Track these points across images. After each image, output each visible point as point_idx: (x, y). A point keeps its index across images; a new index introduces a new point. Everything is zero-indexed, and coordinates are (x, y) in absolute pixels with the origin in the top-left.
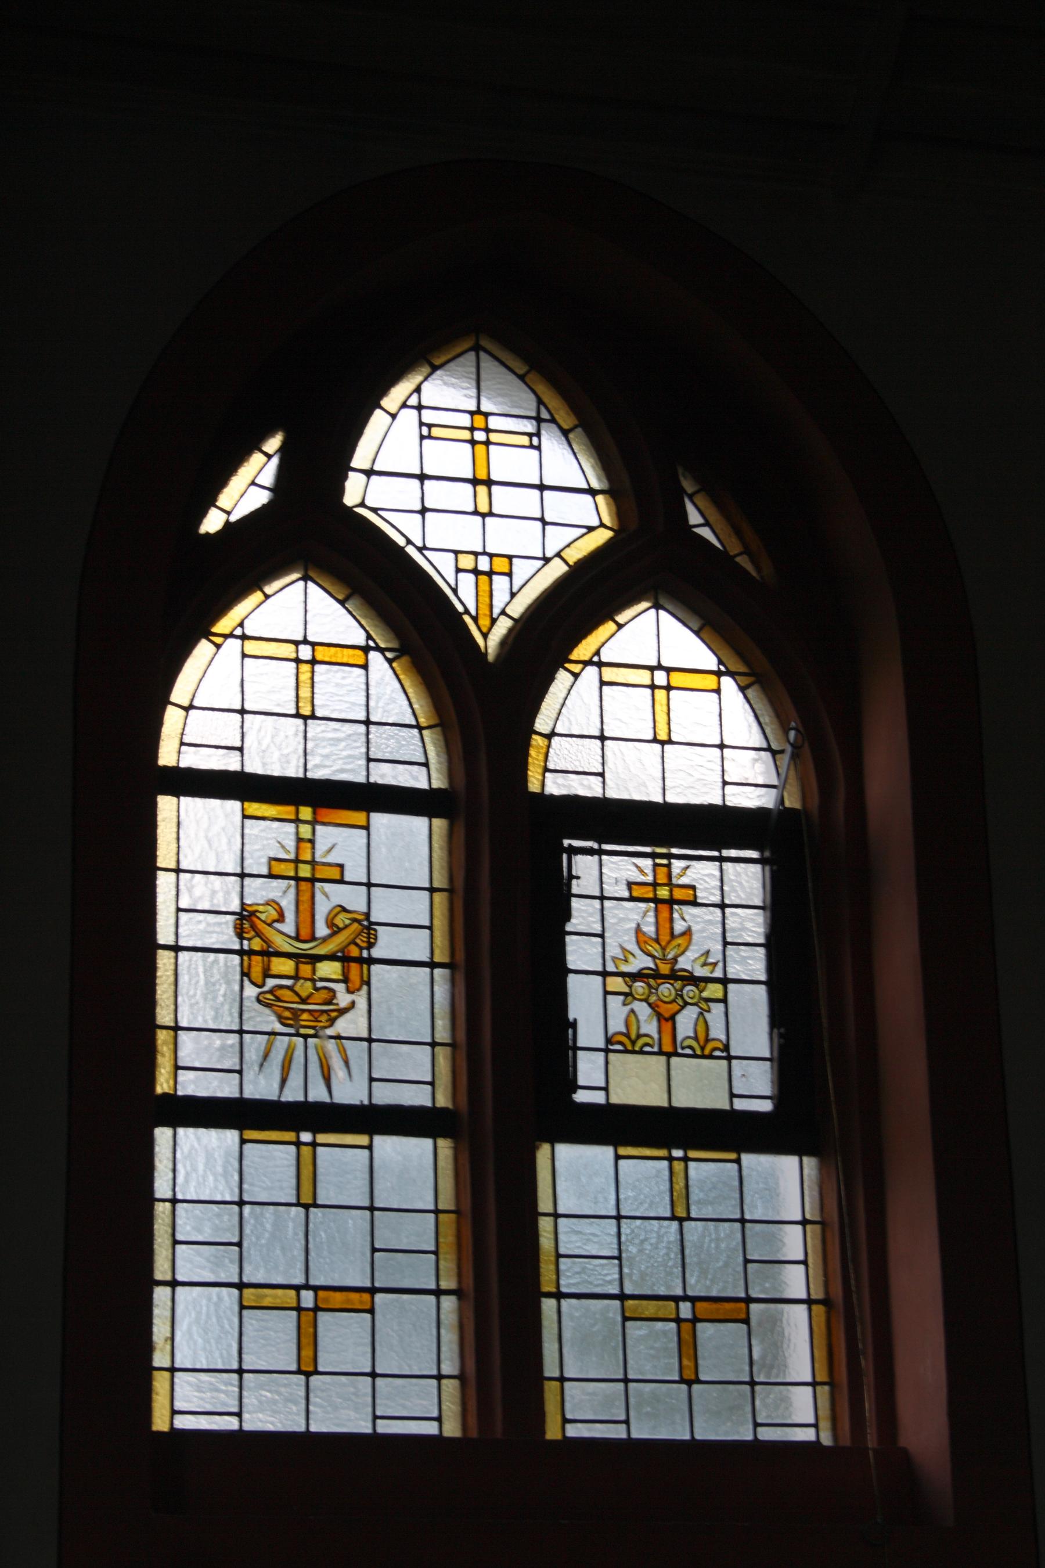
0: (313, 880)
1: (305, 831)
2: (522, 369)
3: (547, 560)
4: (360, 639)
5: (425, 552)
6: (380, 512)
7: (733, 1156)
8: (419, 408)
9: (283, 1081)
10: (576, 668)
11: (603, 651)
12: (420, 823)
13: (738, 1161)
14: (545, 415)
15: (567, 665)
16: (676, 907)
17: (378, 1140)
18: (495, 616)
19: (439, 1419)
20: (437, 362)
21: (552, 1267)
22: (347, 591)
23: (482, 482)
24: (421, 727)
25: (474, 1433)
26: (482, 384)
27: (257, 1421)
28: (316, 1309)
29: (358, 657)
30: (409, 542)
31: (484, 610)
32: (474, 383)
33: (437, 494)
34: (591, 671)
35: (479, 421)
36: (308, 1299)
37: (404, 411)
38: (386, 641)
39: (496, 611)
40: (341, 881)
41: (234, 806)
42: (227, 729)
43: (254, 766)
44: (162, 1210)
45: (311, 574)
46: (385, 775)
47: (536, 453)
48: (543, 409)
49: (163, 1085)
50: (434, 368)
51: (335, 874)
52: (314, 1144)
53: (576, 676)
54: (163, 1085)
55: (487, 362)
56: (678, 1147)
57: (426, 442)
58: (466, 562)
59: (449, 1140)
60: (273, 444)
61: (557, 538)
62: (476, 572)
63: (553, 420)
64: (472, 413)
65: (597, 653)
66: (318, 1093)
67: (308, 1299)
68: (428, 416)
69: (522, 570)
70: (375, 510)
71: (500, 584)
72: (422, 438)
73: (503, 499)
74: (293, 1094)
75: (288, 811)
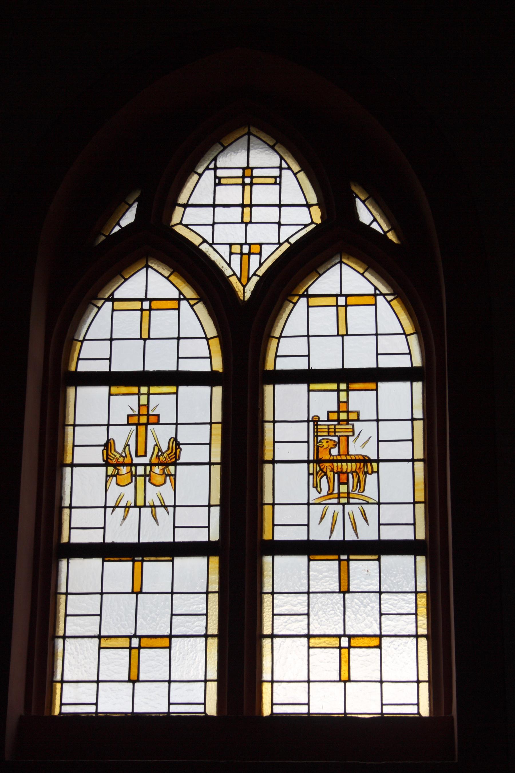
1: (343, 396)
3: (280, 244)
4: (175, 294)
6: (303, 226)
7: (376, 557)
8: (216, 168)
9: (332, 531)
11: (309, 289)
18: (250, 276)
21: (64, 619)
25: (432, 716)
28: (139, 648)
31: (244, 274)
33: (221, 214)
34: (109, 304)
36: (135, 642)
37: (207, 172)
38: (389, 291)
43: (316, 365)
45: (150, 264)
49: (267, 536)
50: (225, 148)
54: (267, 536)
55: (252, 138)
57: (218, 188)
61: (286, 232)
62: (242, 254)
63: (289, 168)
64: (244, 169)
66: (350, 536)
68: (220, 173)
69: (267, 250)
70: (186, 226)
71: (255, 260)
72: (216, 185)
73: (258, 214)
74: (337, 536)
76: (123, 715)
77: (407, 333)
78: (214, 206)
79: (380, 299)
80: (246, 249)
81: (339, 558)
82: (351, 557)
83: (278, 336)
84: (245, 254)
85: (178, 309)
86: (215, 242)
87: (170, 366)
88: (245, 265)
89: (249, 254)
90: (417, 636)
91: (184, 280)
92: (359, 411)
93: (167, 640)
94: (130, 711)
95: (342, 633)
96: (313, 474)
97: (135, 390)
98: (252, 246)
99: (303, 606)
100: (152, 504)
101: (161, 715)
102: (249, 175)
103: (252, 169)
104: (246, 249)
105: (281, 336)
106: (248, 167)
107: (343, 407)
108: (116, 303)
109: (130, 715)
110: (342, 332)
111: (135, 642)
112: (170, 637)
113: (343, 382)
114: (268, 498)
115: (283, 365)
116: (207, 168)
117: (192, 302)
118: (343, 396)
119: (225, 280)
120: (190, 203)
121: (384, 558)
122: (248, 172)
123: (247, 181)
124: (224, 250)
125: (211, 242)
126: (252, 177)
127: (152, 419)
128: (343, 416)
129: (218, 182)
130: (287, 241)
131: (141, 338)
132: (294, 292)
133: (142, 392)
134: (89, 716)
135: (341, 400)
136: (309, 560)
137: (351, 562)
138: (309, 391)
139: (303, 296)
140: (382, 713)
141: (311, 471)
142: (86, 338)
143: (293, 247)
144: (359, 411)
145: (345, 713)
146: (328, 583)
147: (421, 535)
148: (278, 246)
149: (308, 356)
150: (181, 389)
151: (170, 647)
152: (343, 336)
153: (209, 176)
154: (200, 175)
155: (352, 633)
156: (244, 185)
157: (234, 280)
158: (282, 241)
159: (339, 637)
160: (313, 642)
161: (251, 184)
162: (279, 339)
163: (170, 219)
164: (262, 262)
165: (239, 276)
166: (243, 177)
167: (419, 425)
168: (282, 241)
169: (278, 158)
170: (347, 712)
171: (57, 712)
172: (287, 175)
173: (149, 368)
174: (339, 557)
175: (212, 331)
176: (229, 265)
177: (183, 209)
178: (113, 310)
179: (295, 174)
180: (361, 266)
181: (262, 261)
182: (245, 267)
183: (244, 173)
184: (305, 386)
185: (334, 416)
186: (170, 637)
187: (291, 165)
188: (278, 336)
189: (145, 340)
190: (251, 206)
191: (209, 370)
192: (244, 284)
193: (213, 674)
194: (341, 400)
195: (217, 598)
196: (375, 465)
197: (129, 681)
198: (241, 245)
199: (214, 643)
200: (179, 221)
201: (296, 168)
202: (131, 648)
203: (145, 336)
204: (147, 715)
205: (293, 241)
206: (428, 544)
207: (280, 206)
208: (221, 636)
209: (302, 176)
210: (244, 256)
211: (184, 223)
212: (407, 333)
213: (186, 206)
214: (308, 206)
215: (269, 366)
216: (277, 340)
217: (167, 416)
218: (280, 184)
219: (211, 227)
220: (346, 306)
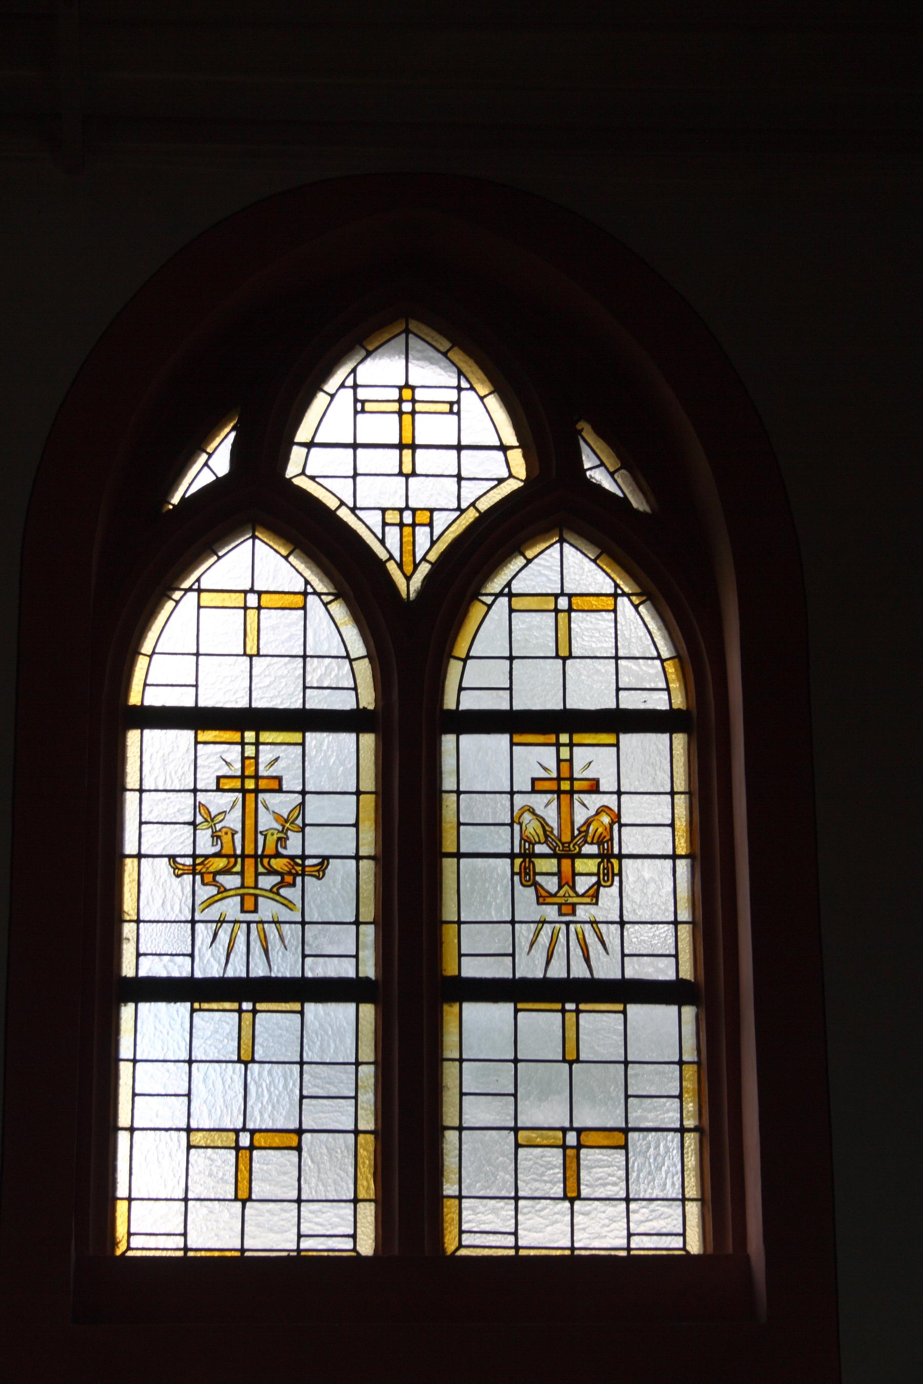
0: (257, 791)
1: (565, 753)
2: (445, 345)
3: (461, 511)
5: (357, 512)
6: (317, 480)
10: (489, 600)
12: (348, 739)
13: (624, 1012)
14: (464, 384)
15: (480, 598)
18: (417, 561)
19: (354, 1236)
20: (371, 348)
23: (410, 446)
26: (410, 352)
30: (342, 503)
31: (408, 559)
32: (403, 356)
35: (407, 394)
37: (342, 391)
39: (418, 558)
40: (280, 790)
41: (188, 735)
42: (497, 674)
44: (122, 1206)
45: (257, 534)
46: (318, 701)
47: (456, 417)
50: (369, 354)
51: (274, 785)
52: (254, 1012)
53: (490, 607)
55: (413, 340)
56: (571, 1001)
57: (359, 416)
58: (392, 517)
61: (470, 491)
63: (472, 388)
64: (401, 388)
65: (509, 585)
66: (579, 971)
68: (362, 394)
69: (441, 521)
70: (313, 478)
71: (422, 534)
72: (356, 412)
73: (426, 461)
74: (557, 971)
75: (235, 736)
86: (358, 506)
89: (414, 525)
92: (282, 777)
96: (517, 874)
97: (552, 738)
98: (418, 513)
99: (268, 1086)
100: (592, 919)
103: (413, 388)
104: (408, 518)
105: (468, 657)
106: (407, 386)
107: (250, 771)
110: (564, 652)
113: (564, 732)
114: (449, 914)
115: (470, 702)
117: (327, 599)
118: (565, 753)
122: (407, 394)
123: (407, 407)
124: (374, 519)
125: (351, 505)
126: (414, 401)
130: (473, 504)
131: (557, 656)
135: (562, 757)
140: (298, 1250)
142: (472, 654)
143: (483, 517)
144: (282, 777)
145: (243, 1250)
146: (177, 1049)
148: (458, 513)
150: (624, 738)
152: (251, 657)
156: (400, 413)
157: (392, 567)
158: (464, 505)
162: (465, 661)
166: (400, 401)
167: (368, 802)
168: (464, 505)
170: (246, 1247)
172: (469, 398)
173: (573, 703)
175: (358, 648)
176: (382, 542)
177: (305, 450)
178: (511, 611)
179: (482, 399)
180: (284, 545)
181: (380, 536)
182: (408, 548)
188: (463, 656)
190: (414, 447)
192: (408, 574)
194: (562, 757)
196: (615, 862)
198: (401, 511)
205: (483, 505)
209: (493, 402)
211: (308, 472)
213: (310, 445)
216: (461, 663)
218: (458, 414)
220: (259, 608)
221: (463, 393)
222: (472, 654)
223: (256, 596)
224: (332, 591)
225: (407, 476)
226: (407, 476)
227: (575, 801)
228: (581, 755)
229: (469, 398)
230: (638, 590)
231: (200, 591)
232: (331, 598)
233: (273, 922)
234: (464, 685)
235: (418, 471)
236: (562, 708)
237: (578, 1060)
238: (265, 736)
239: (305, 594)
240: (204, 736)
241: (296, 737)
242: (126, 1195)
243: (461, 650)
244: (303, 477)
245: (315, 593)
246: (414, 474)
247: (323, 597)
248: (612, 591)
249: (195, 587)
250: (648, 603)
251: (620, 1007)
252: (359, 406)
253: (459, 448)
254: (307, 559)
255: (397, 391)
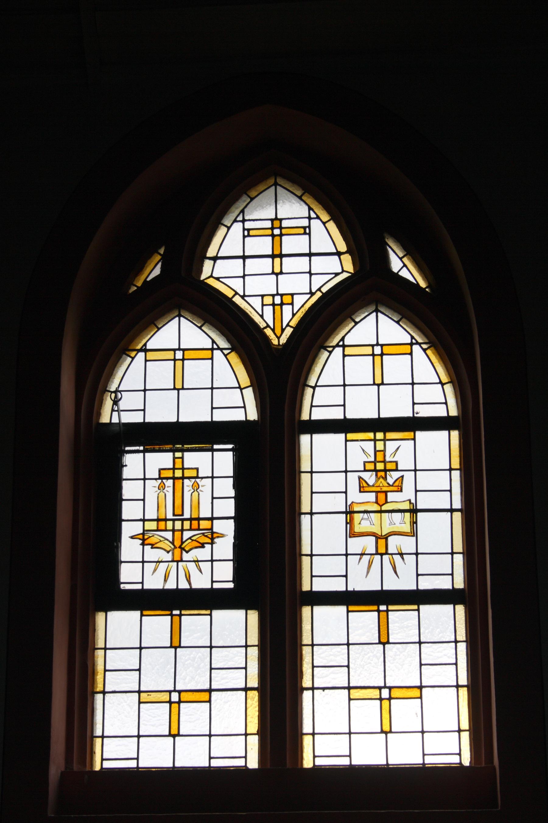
1: (380, 446)
2: (299, 193)
3: (312, 294)
5: (246, 298)
6: (334, 275)
8: (244, 221)
10: (330, 349)
15: (127, 353)
16: (388, 473)
17: (422, 607)
18: (284, 327)
22: (400, 317)
24: (443, 383)
27: (396, 759)
29: (407, 349)
30: (236, 293)
33: (252, 265)
36: (385, 693)
37: (235, 224)
38: (423, 340)
39: (284, 325)
41: (341, 437)
42: (336, 396)
45: (380, 309)
46: (424, 412)
48: (311, 212)
49: (306, 587)
54: (306, 587)
59: (462, 605)
60: (162, 251)
61: (317, 282)
62: (274, 305)
63: (318, 217)
64: (272, 220)
65: (343, 339)
67: (175, 697)
68: (248, 225)
69: (299, 301)
70: (218, 279)
71: (287, 310)
72: (244, 237)
73: (289, 264)
76: (218, 769)
77: (242, 387)
78: (310, 255)
79: (217, 353)
80: (278, 300)
81: (180, 613)
82: (183, 612)
83: (313, 385)
84: (278, 305)
85: (411, 354)
87: (406, 412)
88: (277, 316)
89: (282, 304)
90: (246, 689)
91: (218, 332)
93: (207, 694)
94: (171, 765)
95: (383, 685)
101: (341, 767)
102: (278, 226)
103: (281, 220)
104: (278, 300)
105: (316, 386)
106: (276, 218)
107: (380, 457)
108: (148, 354)
109: (207, 769)
111: (385, 693)
112: (210, 691)
115: (318, 415)
116: (235, 221)
117: (226, 352)
118: (380, 446)
119: (260, 331)
120: (219, 255)
121: (215, 613)
123: (277, 232)
124: (256, 303)
125: (242, 294)
126: (281, 228)
127: (389, 466)
128: (380, 466)
129: (247, 233)
130: (319, 289)
131: (374, 384)
132: (131, 348)
133: (377, 438)
134: (205, 770)
136: (142, 615)
137: (390, 613)
138: (346, 441)
139: (141, 350)
141: (348, 521)
142: (318, 384)
147: (460, 584)
148: (309, 296)
149: (344, 405)
151: (210, 701)
153: (237, 228)
154: (229, 228)
155: (391, 685)
156: (273, 236)
157: (268, 332)
158: (313, 291)
159: (380, 688)
160: (355, 693)
161: (281, 235)
162: (314, 388)
163: (200, 271)
164: (295, 312)
165: (272, 327)
166: (272, 228)
168: (313, 291)
169: (306, 208)
171: (97, 768)
172: (316, 225)
173: (384, 415)
174: (378, 608)
176: (262, 316)
177: (212, 262)
178: (344, 356)
179: (324, 223)
183: (272, 224)
184: (342, 436)
185: (370, 466)
186: (210, 691)
187: (319, 214)
188: (313, 385)
189: (178, 390)
191: (210, 420)
193: (253, 727)
195: (257, 652)
197: (170, 735)
198: (273, 296)
199: (254, 696)
200: (210, 274)
201: (325, 217)
202: (170, 702)
203: (179, 386)
204: (117, 770)
205: (324, 290)
206: (467, 592)
207: (244, 258)
208: (261, 689)
209: (332, 226)
210: (276, 307)
212: (242, 387)
213: (215, 259)
214: (339, 254)
215: (305, 416)
217: (405, 462)
218: (309, 234)
219: (242, 279)
220: (183, 360)
221: (312, 221)
222: (318, 384)
223: (182, 352)
224: (427, 341)
225: (277, 275)
226: (277, 275)
227: (388, 475)
228: (391, 446)
229: (316, 225)
230: (427, 341)
231: (344, 346)
232: (229, 351)
233: (399, 554)
234: (313, 404)
235: (284, 271)
236: (308, 419)
237: (388, 642)
238: (390, 435)
239: (212, 349)
240: (350, 436)
241: (410, 435)
242: (462, 734)
243: (312, 382)
244: (211, 279)
245: (219, 348)
246: (281, 273)
247: (224, 351)
248: (409, 342)
249: (341, 343)
250: (432, 348)
251: (415, 607)
252: (307, 231)
253: (244, 258)
254: (343, 325)
255: (270, 222)
